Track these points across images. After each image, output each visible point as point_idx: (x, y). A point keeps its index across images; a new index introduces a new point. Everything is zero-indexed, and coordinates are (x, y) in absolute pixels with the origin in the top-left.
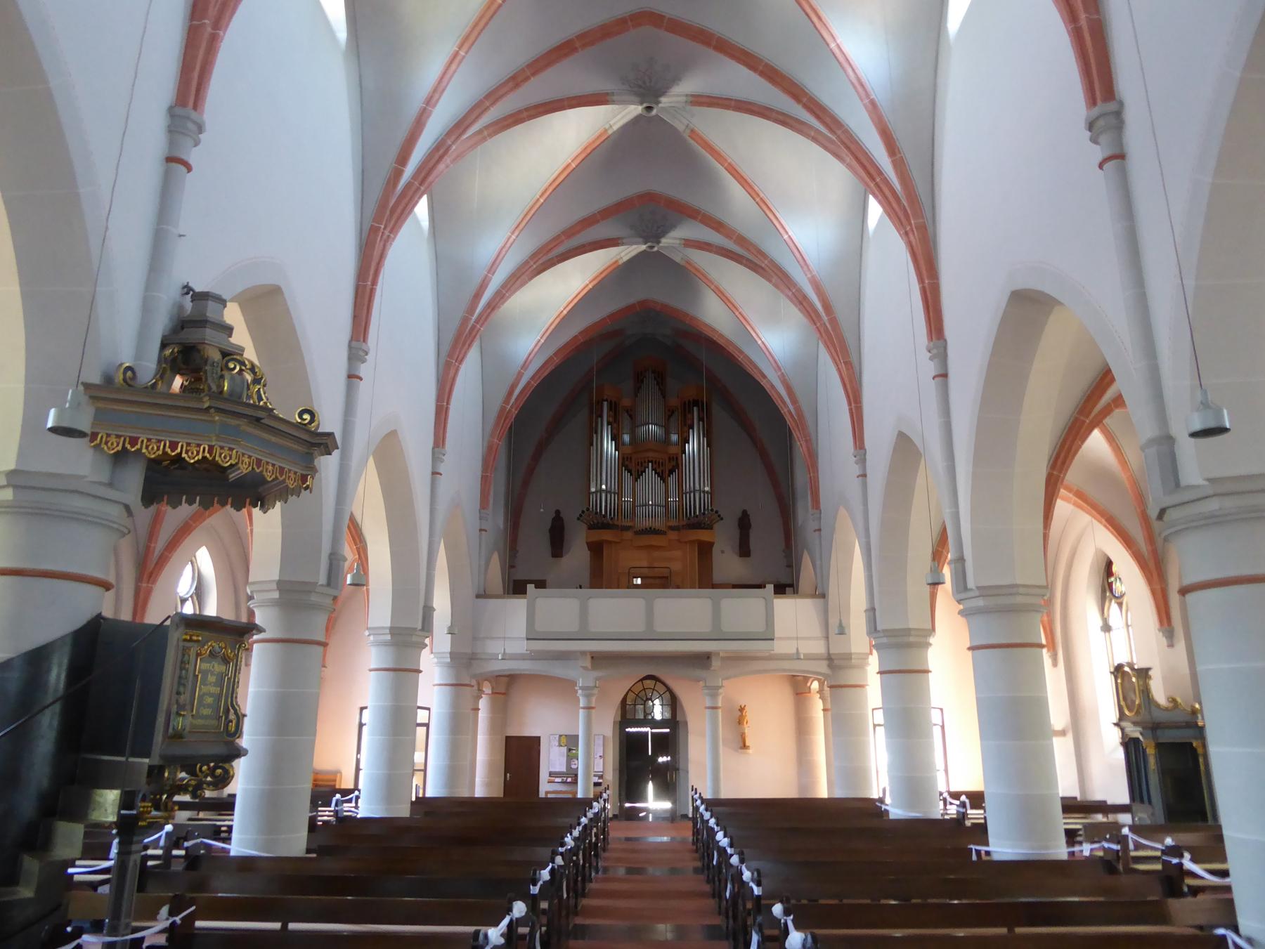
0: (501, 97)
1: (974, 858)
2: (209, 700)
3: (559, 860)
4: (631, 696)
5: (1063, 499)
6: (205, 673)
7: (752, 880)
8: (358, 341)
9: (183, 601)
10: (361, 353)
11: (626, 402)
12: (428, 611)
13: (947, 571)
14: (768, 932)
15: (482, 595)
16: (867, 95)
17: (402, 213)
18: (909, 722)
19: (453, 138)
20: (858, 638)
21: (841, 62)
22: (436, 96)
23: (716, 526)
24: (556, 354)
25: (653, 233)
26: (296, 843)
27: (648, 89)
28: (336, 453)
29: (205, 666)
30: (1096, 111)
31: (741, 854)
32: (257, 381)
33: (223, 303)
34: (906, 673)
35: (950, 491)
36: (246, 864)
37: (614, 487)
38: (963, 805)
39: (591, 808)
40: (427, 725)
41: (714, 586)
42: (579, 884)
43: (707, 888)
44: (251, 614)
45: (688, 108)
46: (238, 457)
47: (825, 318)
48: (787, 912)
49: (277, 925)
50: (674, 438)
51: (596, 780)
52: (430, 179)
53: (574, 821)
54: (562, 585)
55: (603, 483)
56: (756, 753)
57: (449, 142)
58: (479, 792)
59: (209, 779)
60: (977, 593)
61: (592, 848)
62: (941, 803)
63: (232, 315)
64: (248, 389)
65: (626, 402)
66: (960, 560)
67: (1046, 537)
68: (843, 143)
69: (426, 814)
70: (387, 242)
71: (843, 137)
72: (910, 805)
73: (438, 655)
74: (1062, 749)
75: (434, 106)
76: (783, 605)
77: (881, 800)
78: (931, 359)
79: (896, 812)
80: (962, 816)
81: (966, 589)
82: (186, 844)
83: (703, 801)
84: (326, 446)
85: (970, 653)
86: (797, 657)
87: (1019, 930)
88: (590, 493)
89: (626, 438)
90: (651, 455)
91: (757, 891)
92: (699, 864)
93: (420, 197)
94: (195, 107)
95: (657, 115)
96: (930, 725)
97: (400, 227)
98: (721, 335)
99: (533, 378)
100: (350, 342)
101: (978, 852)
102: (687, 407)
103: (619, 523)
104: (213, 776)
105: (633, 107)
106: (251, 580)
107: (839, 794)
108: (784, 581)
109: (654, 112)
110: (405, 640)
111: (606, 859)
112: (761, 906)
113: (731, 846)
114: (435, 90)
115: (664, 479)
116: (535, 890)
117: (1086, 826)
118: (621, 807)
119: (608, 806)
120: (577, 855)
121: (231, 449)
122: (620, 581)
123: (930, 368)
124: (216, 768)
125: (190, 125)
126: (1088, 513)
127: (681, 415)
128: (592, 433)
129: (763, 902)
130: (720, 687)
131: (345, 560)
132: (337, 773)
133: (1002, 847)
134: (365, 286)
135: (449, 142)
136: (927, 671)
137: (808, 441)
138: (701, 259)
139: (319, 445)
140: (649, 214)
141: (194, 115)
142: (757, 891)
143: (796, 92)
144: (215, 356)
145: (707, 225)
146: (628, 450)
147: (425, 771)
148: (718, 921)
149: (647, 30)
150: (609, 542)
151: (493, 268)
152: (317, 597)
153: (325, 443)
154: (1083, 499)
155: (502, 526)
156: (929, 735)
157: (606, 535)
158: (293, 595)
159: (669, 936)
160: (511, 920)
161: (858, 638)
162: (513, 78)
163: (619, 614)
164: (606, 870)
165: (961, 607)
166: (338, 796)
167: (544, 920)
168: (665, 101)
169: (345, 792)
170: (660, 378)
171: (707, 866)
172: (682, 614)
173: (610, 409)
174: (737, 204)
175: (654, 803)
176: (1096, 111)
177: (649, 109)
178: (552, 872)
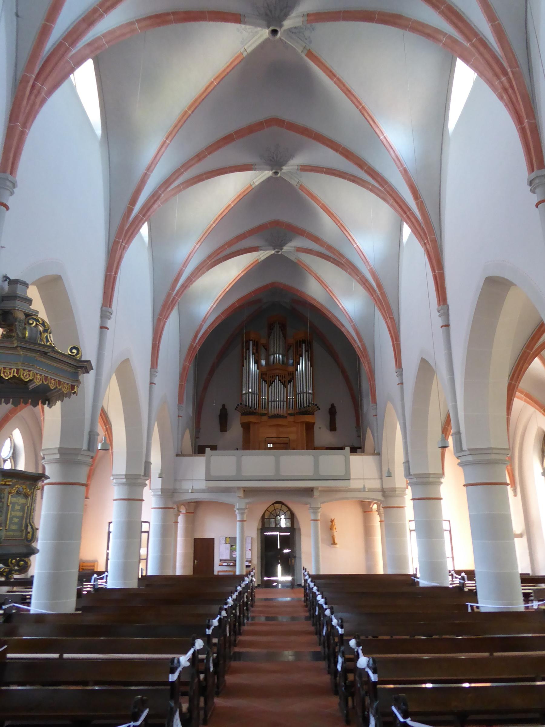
0: (190, 167)
1: (470, 610)
2: (16, 520)
3: (224, 613)
4: (267, 513)
5: (518, 398)
6: (13, 504)
7: (338, 625)
8: (107, 307)
9: (5, 461)
10: (108, 314)
11: (263, 341)
12: (148, 464)
13: (450, 440)
14: (347, 656)
15: (179, 455)
16: (402, 165)
17: (132, 234)
18: (430, 529)
19: (162, 190)
20: (400, 479)
21: (387, 146)
22: (153, 166)
23: (315, 413)
24: (222, 313)
25: (279, 244)
26: (69, 605)
27: (276, 162)
28: (92, 372)
29: (14, 500)
30: (534, 175)
31: (331, 609)
32: (46, 331)
33: (26, 285)
34: (428, 500)
35: (450, 394)
36: (40, 618)
37: (257, 391)
38: (463, 578)
39: (244, 581)
40: (148, 532)
41: (315, 448)
42: (237, 627)
43: (312, 629)
44: (44, 468)
45: (299, 172)
46: (34, 375)
47: (378, 292)
48: (358, 645)
49: (56, 656)
50: (291, 362)
51: (247, 564)
52: (149, 213)
53: (234, 589)
54: (225, 448)
55: (250, 388)
56: (341, 548)
57: (160, 192)
58: (179, 572)
59: (16, 568)
60: (468, 453)
61: (245, 605)
62: (450, 577)
63: (32, 292)
64: (41, 333)
65: (263, 341)
66: (458, 433)
67: (508, 420)
68: (388, 192)
69: (147, 586)
70: (124, 249)
71: (388, 189)
72: (432, 579)
73: (154, 490)
74: (520, 545)
75: (152, 171)
76: (356, 460)
77: (415, 575)
78: (440, 316)
79: (423, 583)
80: (463, 585)
81: (462, 450)
82: (4, 607)
83: (310, 576)
84: (86, 368)
85: (465, 488)
86: (363, 490)
87: (496, 654)
88: (242, 394)
89: (263, 362)
90: (277, 371)
91: (341, 631)
92: (308, 614)
93: (143, 224)
94: (11, 173)
95: (280, 177)
96: (442, 531)
97: (132, 241)
98: (318, 303)
99: (209, 327)
100: (102, 308)
101: (472, 607)
102: (299, 344)
103: (260, 412)
104: (18, 566)
105: (266, 172)
106: (43, 448)
107: (390, 572)
108: (356, 445)
109: (279, 175)
110: (134, 482)
111: (253, 612)
112: (343, 640)
113: (326, 603)
114: (152, 163)
115: (285, 386)
116: (209, 632)
117: (536, 591)
118: (262, 581)
119: (254, 579)
120: (235, 609)
121: (30, 371)
122: (261, 446)
123: (439, 321)
124: (20, 561)
125: (8, 183)
126: (533, 406)
127: (295, 349)
128: (244, 359)
129: (345, 638)
130: (319, 508)
131: (98, 435)
132: (95, 562)
133: (486, 604)
134: (110, 276)
135: (160, 192)
136: (441, 499)
137: (369, 363)
138: (307, 259)
139: (81, 368)
140: (276, 233)
141: (10, 177)
142: (341, 631)
143: (361, 163)
144: (21, 316)
145: (309, 238)
146: (264, 369)
147: (147, 559)
148: (319, 649)
149: (275, 128)
150: (254, 423)
151: (185, 264)
152: (82, 458)
153: (84, 366)
154: (530, 398)
155: (191, 414)
156: (442, 537)
157: (252, 419)
158: (67, 457)
159: (291, 658)
160: (195, 651)
161: (400, 479)
162: (197, 156)
163: (260, 465)
164: (253, 618)
165: (459, 461)
166: (95, 576)
167: (215, 650)
168: (285, 169)
169: (100, 573)
170: (283, 328)
171: (313, 616)
172: (297, 465)
173: (254, 345)
174: (327, 228)
175: (281, 577)
176: (534, 175)
177: (276, 173)
178: (220, 621)
